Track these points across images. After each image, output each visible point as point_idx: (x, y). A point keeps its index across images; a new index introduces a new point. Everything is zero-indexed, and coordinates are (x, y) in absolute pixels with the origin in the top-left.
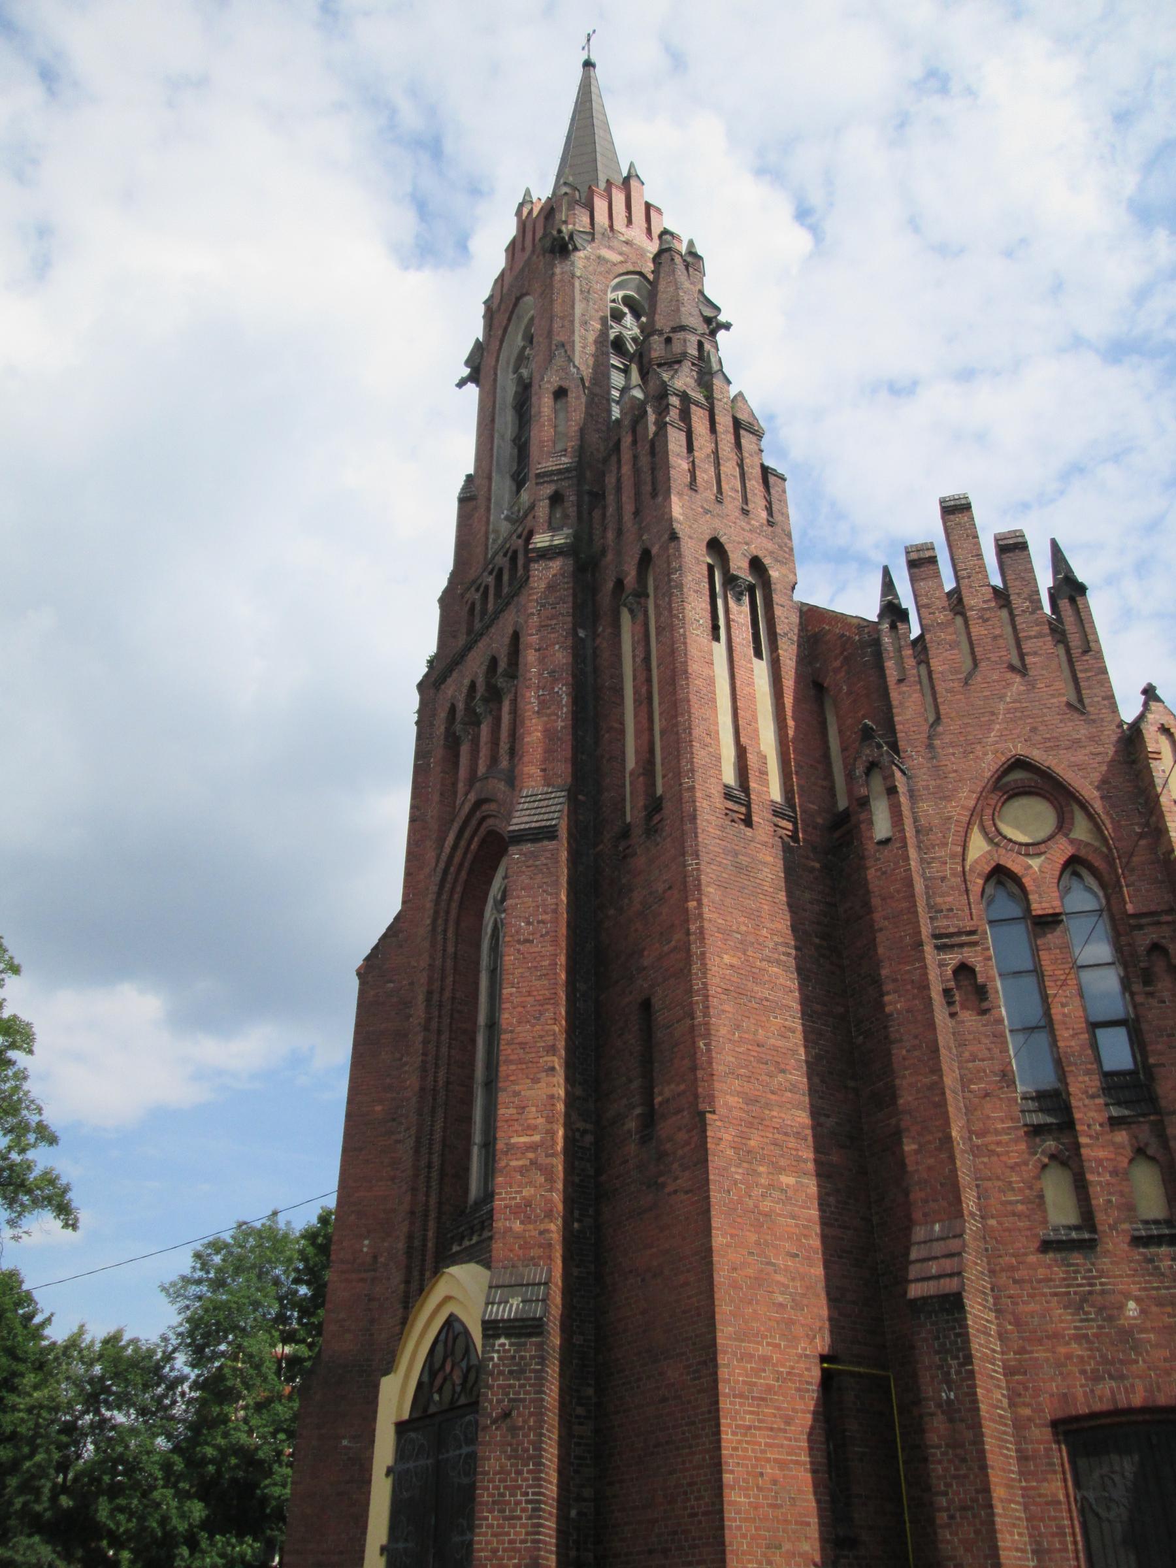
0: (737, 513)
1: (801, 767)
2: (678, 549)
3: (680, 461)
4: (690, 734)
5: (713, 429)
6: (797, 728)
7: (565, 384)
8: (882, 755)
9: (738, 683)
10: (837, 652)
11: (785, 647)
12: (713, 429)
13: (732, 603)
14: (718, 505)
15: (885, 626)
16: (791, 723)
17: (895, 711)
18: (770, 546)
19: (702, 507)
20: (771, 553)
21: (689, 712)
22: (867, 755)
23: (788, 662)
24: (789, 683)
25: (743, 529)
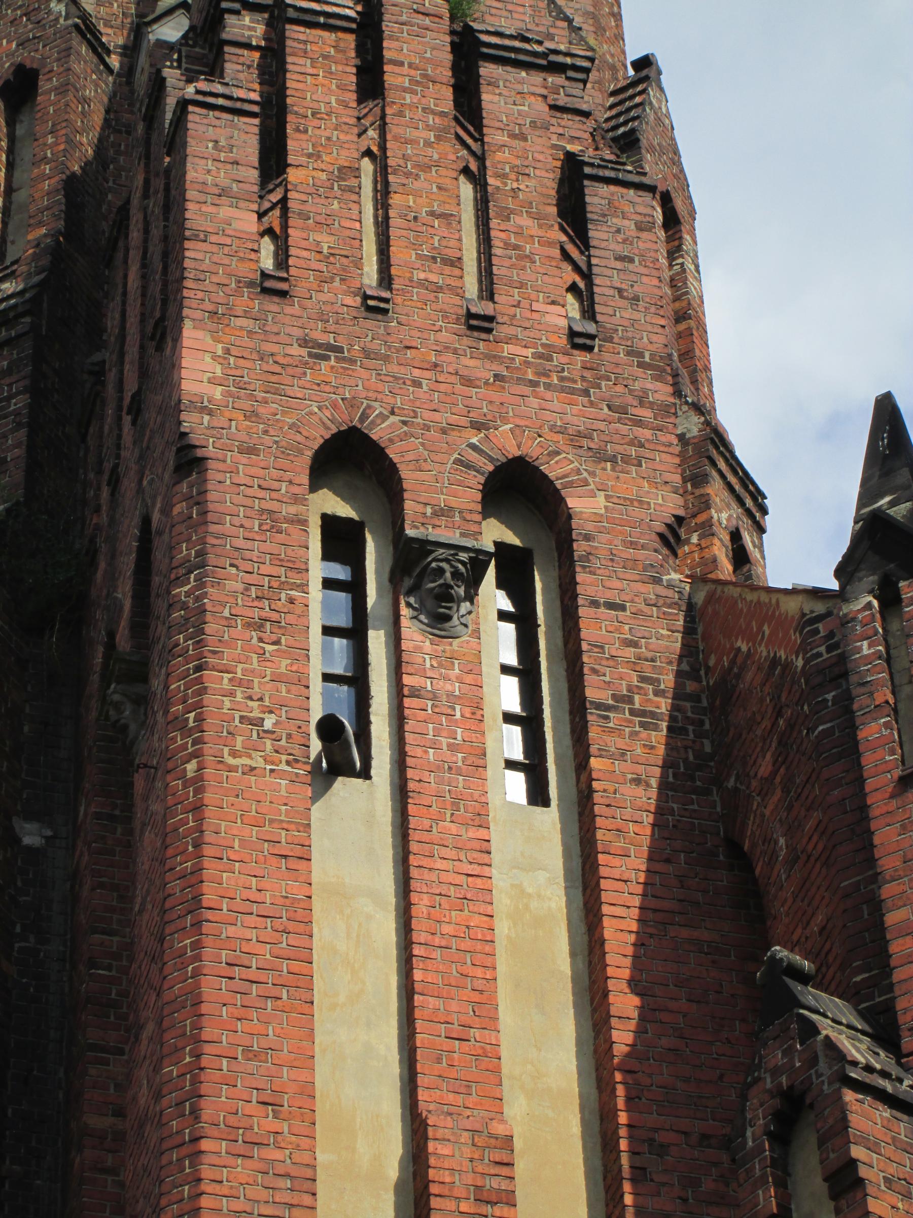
0: (449, 333)
1: (662, 1150)
2: (199, 500)
3: (225, 212)
4: (195, 1113)
5: (370, 82)
6: (646, 1016)
7: (30, 57)
8: (813, 1061)
9: (421, 904)
10: (766, 723)
11: (614, 743)
12: (370, 82)
13: (413, 632)
14: (372, 324)
15: (865, 602)
16: (625, 1004)
17: (887, 891)
18: (576, 414)
19: (304, 342)
20: (577, 438)
21: (197, 1040)
22: (776, 1072)
23: (629, 791)
24: (626, 868)
25: (468, 382)
